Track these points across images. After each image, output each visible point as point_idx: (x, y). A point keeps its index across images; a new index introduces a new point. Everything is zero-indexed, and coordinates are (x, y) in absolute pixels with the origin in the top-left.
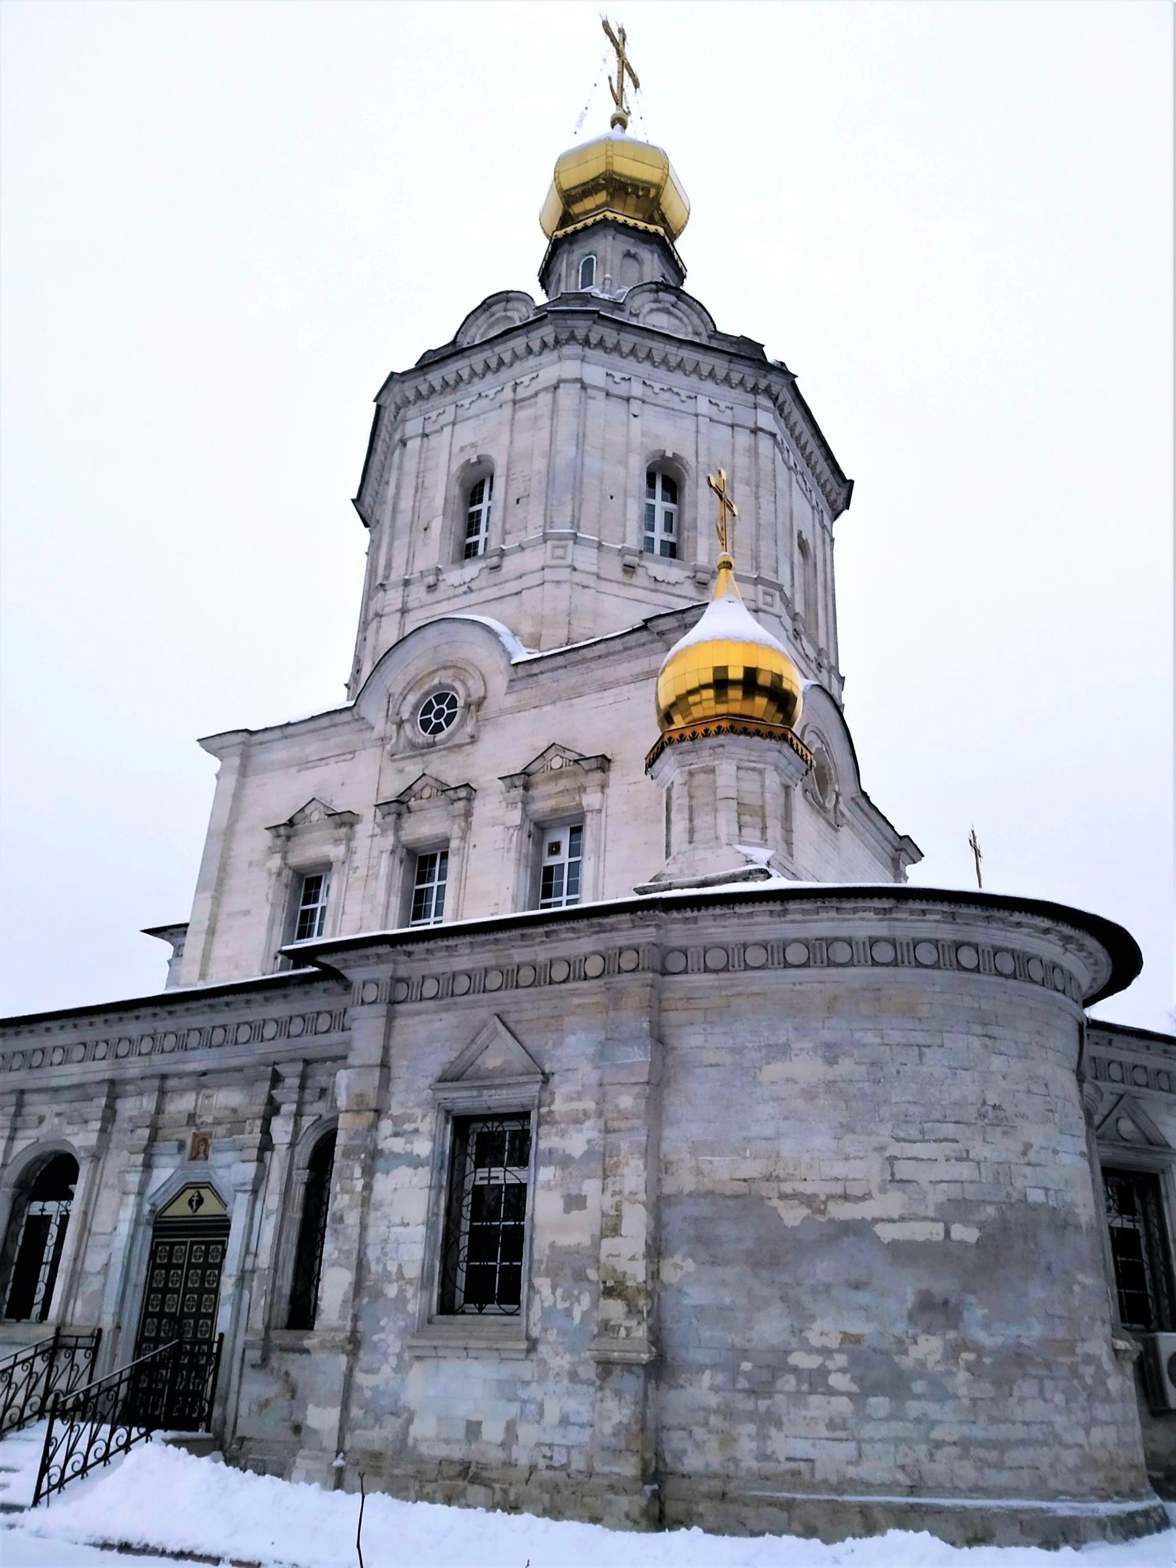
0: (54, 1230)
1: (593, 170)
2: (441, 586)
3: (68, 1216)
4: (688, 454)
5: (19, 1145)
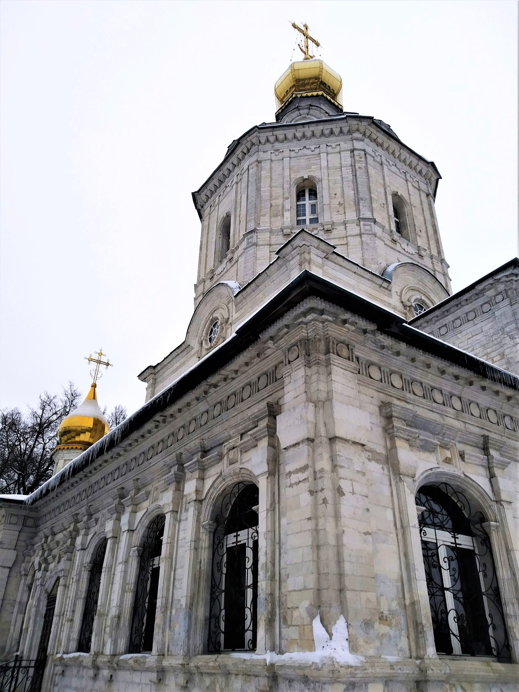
0: (249, 553)
1: (289, 83)
2: (215, 277)
4: (316, 174)
5: (208, 483)
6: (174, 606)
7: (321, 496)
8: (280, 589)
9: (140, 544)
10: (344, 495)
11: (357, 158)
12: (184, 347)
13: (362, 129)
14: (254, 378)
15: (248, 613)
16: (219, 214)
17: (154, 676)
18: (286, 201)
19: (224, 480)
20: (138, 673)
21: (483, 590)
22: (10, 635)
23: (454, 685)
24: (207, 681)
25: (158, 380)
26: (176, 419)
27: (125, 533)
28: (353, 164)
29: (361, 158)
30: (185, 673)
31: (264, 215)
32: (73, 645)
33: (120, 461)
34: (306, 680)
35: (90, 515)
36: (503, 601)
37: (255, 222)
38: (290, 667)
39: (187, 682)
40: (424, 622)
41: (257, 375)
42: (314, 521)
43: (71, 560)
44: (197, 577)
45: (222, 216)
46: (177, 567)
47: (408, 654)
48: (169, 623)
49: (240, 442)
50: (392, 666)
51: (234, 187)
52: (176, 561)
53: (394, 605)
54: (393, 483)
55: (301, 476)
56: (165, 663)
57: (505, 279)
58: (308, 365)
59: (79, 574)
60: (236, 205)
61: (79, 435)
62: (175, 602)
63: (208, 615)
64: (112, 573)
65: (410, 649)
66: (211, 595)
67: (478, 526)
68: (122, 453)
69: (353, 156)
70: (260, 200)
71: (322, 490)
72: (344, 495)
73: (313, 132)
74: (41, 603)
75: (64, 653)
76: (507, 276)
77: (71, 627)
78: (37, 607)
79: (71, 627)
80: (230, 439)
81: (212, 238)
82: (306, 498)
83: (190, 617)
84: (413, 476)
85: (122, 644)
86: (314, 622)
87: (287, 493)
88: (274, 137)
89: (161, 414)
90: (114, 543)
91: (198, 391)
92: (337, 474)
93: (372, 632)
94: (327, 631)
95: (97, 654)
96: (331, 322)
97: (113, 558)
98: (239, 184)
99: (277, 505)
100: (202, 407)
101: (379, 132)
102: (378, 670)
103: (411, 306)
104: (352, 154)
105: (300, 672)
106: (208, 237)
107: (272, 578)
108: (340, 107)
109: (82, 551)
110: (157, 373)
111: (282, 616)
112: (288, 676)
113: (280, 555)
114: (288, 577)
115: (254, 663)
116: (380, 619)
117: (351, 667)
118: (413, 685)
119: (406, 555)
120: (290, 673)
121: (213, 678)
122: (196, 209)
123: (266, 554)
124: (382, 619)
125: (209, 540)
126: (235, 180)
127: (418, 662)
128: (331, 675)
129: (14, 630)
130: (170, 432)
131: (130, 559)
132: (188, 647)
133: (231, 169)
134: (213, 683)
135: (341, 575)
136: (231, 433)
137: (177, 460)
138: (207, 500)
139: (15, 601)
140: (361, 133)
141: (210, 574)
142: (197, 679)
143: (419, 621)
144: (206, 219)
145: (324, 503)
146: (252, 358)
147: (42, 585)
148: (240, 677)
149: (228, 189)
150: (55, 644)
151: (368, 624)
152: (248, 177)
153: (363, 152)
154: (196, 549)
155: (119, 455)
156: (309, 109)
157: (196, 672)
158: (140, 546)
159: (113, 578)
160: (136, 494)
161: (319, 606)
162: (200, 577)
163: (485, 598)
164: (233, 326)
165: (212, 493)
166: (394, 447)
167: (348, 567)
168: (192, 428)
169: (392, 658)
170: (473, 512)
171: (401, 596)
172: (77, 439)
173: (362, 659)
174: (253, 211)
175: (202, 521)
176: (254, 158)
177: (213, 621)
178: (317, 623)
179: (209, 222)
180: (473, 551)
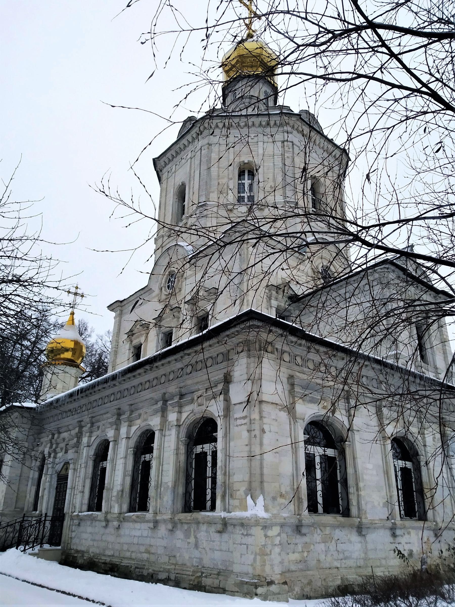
0: (209, 458)
3: (216, 451)
5: (184, 416)
6: (162, 486)
7: (253, 433)
8: (229, 480)
9: (134, 446)
10: (265, 433)
11: (286, 149)
12: (146, 289)
13: (291, 123)
14: (215, 355)
15: (209, 491)
16: (176, 181)
17: (151, 525)
18: (231, 181)
19: (195, 415)
20: (138, 524)
21: (339, 479)
22: (27, 500)
23: (316, 528)
24: (186, 527)
25: (124, 311)
26: (159, 369)
27: (124, 439)
28: (283, 153)
29: (289, 148)
30: (172, 523)
31: (213, 192)
32: (85, 507)
33: (116, 389)
34: (242, 525)
35: (92, 424)
36: (348, 485)
37: (206, 197)
38: (234, 519)
39: (173, 528)
40: (303, 497)
41: (217, 353)
42: (249, 446)
43: (77, 452)
44: (178, 470)
45: (178, 184)
46: (164, 463)
47: (294, 513)
48: (160, 496)
49: (205, 395)
50: (285, 519)
51: (189, 161)
52: (163, 460)
53: (288, 489)
54: (292, 423)
55: (243, 421)
56: (158, 518)
57: (379, 270)
58: (249, 357)
59: (86, 463)
60: (190, 178)
61: (64, 353)
62: (163, 484)
63: (184, 492)
64: (114, 463)
65: (295, 510)
66: (186, 480)
67: (339, 444)
68: (117, 384)
69: (283, 147)
70: (210, 179)
71: (254, 430)
72: (265, 433)
73: (253, 122)
74: (53, 479)
75: (79, 512)
76: (381, 269)
77: (83, 496)
78: (50, 482)
79: (83, 496)
80: (199, 391)
81: (170, 200)
82: (245, 434)
83: (174, 492)
84: (303, 419)
85: (125, 507)
86: (248, 497)
87: (235, 430)
88: (223, 124)
89: (150, 365)
90: (115, 445)
91: (178, 356)
92: (263, 422)
93: (276, 502)
94: (254, 502)
95: (107, 513)
96: (263, 332)
97: (114, 454)
98: (193, 159)
99: (228, 434)
100: (179, 365)
101: (304, 125)
102: (278, 520)
103: (319, 271)
104: (283, 144)
105: (240, 521)
106: (166, 198)
107: (225, 474)
108: (276, 85)
109: (88, 448)
110: (123, 306)
111: (230, 494)
112: (233, 523)
113: (229, 462)
114: (234, 474)
115: (214, 518)
116: (280, 496)
117: (265, 519)
118: (295, 527)
119: (296, 463)
120: (234, 522)
121: (189, 525)
122: (155, 170)
123: (222, 461)
124: (282, 496)
125: (185, 448)
126: (189, 157)
127: (298, 517)
128: (255, 522)
129: (30, 497)
130: (154, 377)
131: (128, 456)
132: (173, 509)
133: (186, 144)
134: (189, 528)
135: (262, 475)
136: (200, 387)
137: (162, 398)
138: (183, 426)
139: (29, 477)
140: (291, 127)
141: (186, 468)
142: (179, 526)
143: (300, 497)
144: (164, 183)
145: (255, 437)
146: (215, 344)
147: (53, 467)
148: (205, 524)
149: (183, 161)
150: (70, 506)
151: (274, 499)
152: (201, 156)
153: (291, 144)
154: (177, 454)
155: (115, 385)
156: (251, 99)
157: (179, 522)
158: (134, 448)
159: (115, 467)
160: (131, 415)
161: (250, 490)
162: (179, 470)
163: (339, 485)
164: (187, 281)
165: (187, 422)
166: (294, 403)
167: (265, 471)
168: (171, 377)
169: (285, 515)
170: (337, 436)
171: (292, 484)
172: (62, 356)
173: (270, 515)
174: (204, 188)
175: (180, 437)
176: (205, 141)
177: (188, 495)
178: (249, 498)
179: (167, 185)
180: (335, 458)
